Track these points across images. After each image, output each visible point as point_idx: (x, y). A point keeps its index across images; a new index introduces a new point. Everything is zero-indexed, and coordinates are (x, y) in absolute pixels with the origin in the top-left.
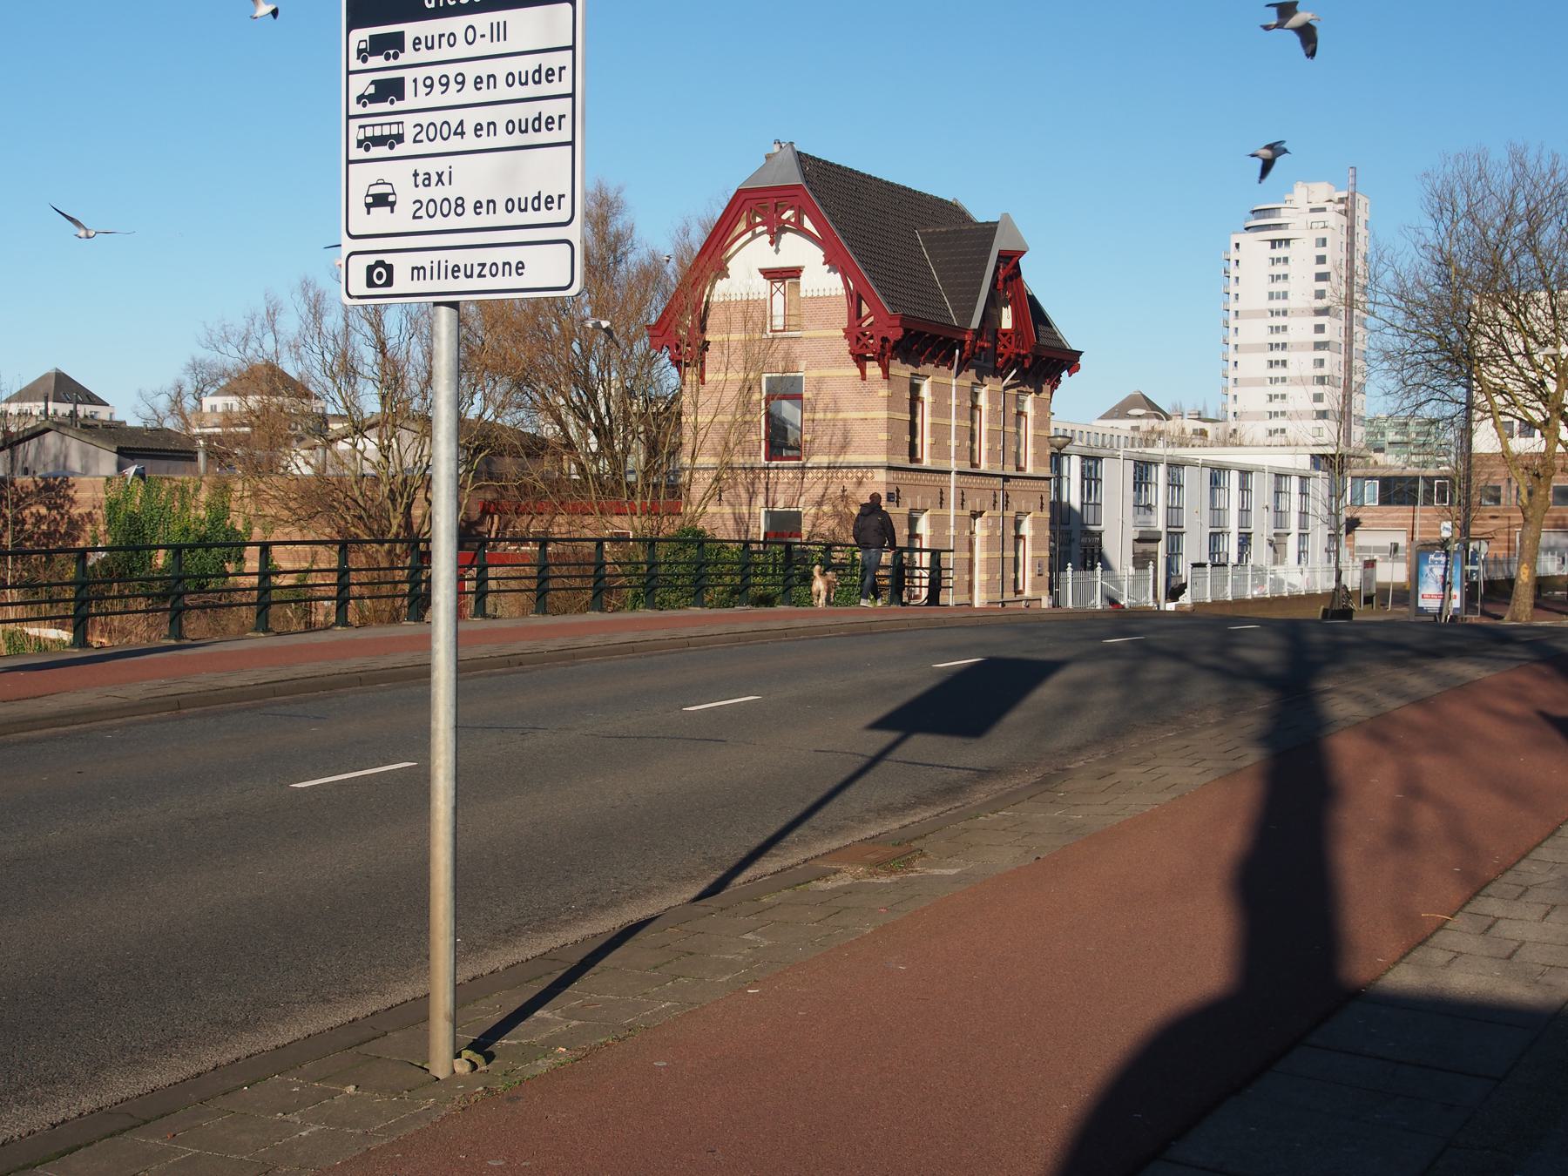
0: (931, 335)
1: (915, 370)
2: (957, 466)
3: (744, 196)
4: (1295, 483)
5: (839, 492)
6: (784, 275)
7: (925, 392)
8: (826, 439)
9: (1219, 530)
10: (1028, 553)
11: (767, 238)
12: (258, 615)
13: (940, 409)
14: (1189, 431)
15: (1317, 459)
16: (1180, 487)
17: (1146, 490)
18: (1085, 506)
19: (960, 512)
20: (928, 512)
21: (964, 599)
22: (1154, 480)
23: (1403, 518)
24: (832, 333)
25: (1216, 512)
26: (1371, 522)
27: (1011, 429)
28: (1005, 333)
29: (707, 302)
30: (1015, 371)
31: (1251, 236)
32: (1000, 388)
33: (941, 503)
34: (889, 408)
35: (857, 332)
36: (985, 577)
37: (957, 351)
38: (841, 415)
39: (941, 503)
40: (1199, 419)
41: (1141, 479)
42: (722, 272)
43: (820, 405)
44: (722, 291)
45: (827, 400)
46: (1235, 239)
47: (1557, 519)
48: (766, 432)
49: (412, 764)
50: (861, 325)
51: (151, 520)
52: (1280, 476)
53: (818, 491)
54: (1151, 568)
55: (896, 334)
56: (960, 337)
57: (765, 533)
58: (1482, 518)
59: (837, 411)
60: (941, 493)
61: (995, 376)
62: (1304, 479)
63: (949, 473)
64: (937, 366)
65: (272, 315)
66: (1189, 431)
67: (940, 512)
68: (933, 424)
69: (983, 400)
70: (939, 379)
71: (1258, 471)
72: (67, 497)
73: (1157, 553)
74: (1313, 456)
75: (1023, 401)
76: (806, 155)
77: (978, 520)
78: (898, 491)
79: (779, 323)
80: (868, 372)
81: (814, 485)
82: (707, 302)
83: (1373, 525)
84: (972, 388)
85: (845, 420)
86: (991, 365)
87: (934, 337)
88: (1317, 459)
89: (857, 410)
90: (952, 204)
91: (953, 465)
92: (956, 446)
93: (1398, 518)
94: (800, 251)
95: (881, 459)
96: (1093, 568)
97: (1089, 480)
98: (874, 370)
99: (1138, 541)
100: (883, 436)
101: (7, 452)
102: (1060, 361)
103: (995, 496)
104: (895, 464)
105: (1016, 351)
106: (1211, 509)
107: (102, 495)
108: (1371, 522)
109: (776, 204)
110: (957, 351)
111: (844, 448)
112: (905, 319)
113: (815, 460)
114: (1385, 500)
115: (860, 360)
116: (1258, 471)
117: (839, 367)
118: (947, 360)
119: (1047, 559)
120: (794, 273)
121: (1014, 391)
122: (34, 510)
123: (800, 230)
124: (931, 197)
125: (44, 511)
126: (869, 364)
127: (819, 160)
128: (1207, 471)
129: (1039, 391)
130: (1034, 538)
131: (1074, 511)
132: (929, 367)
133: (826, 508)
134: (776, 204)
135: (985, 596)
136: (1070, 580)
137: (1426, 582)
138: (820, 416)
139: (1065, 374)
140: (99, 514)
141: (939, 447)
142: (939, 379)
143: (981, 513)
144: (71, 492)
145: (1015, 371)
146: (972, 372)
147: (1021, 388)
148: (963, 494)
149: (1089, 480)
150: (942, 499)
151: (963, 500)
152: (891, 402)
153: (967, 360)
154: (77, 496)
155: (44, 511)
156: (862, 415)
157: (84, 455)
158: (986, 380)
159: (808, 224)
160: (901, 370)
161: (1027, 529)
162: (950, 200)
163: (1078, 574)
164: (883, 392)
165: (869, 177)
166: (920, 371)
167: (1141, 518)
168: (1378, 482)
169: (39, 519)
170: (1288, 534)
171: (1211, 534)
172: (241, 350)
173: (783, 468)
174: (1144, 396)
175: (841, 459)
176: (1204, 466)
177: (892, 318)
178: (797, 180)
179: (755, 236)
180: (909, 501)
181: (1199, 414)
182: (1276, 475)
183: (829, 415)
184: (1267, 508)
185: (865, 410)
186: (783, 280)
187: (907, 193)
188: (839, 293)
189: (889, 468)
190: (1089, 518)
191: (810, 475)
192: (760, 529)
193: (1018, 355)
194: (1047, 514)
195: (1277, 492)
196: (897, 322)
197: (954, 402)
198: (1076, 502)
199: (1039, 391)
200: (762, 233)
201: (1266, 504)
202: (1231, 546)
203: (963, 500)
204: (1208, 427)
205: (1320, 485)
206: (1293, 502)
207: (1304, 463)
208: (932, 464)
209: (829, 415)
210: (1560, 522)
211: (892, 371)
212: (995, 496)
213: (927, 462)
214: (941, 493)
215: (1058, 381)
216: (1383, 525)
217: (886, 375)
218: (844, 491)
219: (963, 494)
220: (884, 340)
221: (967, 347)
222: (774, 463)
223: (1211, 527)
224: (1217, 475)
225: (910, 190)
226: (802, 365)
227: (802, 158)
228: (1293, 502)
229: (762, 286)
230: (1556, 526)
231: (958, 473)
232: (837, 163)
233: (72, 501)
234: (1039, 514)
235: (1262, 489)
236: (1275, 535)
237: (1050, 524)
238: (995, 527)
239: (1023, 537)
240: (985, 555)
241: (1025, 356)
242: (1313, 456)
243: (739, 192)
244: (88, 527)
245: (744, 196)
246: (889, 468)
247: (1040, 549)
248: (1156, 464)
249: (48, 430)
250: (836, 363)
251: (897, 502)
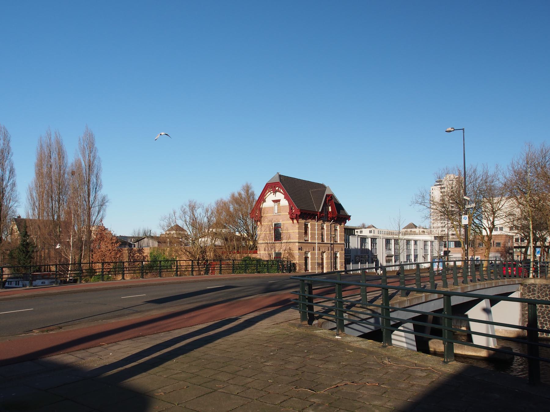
0: (308, 213)
1: (306, 221)
2: (317, 242)
3: (268, 185)
4: (429, 243)
5: (289, 248)
6: (277, 201)
7: (309, 226)
8: (285, 236)
9: (409, 254)
10: (338, 260)
11: (273, 193)
12: (142, 275)
13: (313, 229)
14: (421, 231)
15: (436, 238)
16: (417, 245)
17: (389, 245)
18: (373, 250)
19: (319, 252)
20: (310, 252)
21: (321, 271)
22: (391, 243)
23: (460, 250)
24: (286, 213)
25: (408, 250)
26: (452, 251)
27: (333, 233)
28: (330, 212)
29: (262, 208)
30: (333, 220)
31: (435, 187)
32: (329, 224)
33: (314, 250)
34: (298, 229)
35: (291, 213)
36: (326, 266)
37: (316, 217)
38: (289, 231)
39: (314, 250)
40: (423, 228)
41: (387, 243)
42: (264, 201)
43: (284, 230)
44: (264, 205)
45: (285, 228)
46: (432, 188)
47: (497, 250)
48: (274, 236)
49: (280, 307)
50: (292, 211)
51: (158, 256)
52: (425, 242)
53: (284, 248)
54: (391, 262)
55: (299, 213)
56: (317, 214)
57: (274, 257)
58: (479, 250)
59: (288, 230)
60: (314, 248)
61: (328, 222)
62: (432, 242)
63: (316, 243)
64: (312, 220)
65: (174, 213)
66: (421, 231)
67: (314, 252)
68: (311, 233)
69: (325, 227)
70: (312, 223)
71: (419, 240)
72: (143, 252)
73: (392, 259)
74: (435, 237)
75: (337, 227)
76: (282, 175)
77: (324, 253)
78: (302, 247)
79: (276, 212)
80: (294, 222)
81: (284, 246)
82: (262, 208)
83: (453, 252)
84: (322, 225)
85: (289, 232)
86: (327, 219)
87: (309, 214)
88: (436, 238)
89: (292, 230)
90: (321, 184)
91: (317, 242)
92: (317, 237)
93: (459, 250)
94: (280, 196)
95: (297, 241)
96: (366, 263)
97: (374, 243)
98: (295, 221)
99: (387, 257)
100: (297, 236)
101: (138, 242)
102: (345, 218)
103: (328, 248)
104: (300, 242)
105: (332, 216)
106: (386, 249)
107: (149, 251)
108: (452, 251)
109: (274, 186)
110: (316, 217)
111: (289, 238)
112: (300, 210)
113: (283, 241)
114: (456, 246)
115: (292, 219)
116: (419, 240)
117: (288, 221)
118: (314, 218)
119: (344, 262)
120: (279, 201)
121: (334, 225)
122: (137, 254)
123: (280, 192)
124: (316, 183)
125: (139, 255)
126: (294, 220)
127: (286, 176)
128: (405, 241)
129: (340, 225)
130: (340, 257)
131: (370, 250)
132: (310, 220)
133: (286, 252)
134: (274, 186)
135: (326, 270)
136: (351, 266)
137: (434, 266)
138: (284, 232)
139: (347, 220)
140: (149, 255)
141: (313, 237)
142: (312, 223)
143: (325, 252)
144: (143, 251)
145: (333, 220)
146: (321, 221)
147: (335, 224)
148: (319, 248)
149: (374, 243)
150: (314, 249)
151: (319, 249)
152: (299, 228)
153: (319, 218)
154: (145, 252)
155: (139, 255)
156: (293, 231)
157: (153, 243)
158: (325, 222)
159: (281, 191)
160: (302, 221)
161: (338, 255)
162: (322, 183)
163: (353, 265)
164: (297, 226)
165: (299, 179)
166: (307, 221)
167: (387, 252)
168: (454, 242)
169: (138, 256)
170: (428, 255)
171: (407, 255)
172: (168, 220)
173: (277, 243)
174: (413, 224)
175: (289, 241)
176: (404, 240)
177: (298, 210)
178: (278, 181)
179: (271, 193)
180: (305, 250)
181: (423, 227)
182: (424, 241)
183: (286, 231)
184: (422, 249)
185: (294, 230)
186: (277, 202)
187: (309, 182)
188: (287, 205)
189: (299, 243)
190: (374, 251)
191: (283, 244)
192: (273, 256)
193: (333, 217)
194: (343, 252)
195: (425, 245)
196: (299, 211)
197: (316, 228)
198: (370, 248)
199: (340, 225)
200: (272, 193)
201: (422, 248)
202: (412, 258)
203: (319, 249)
204: (425, 230)
205: (436, 243)
206: (429, 248)
207: (433, 238)
208: (311, 241)
209: (286, 231)
210: (498, 251)
211: (299, 221)
212: (328, 248)
213: (325, 242)
214: (314, 248)
215: (346, 222)
216: (456, 252)
217: (298, 222)
218: (290, 248)
219: (319, 248)
220: (297, 215)
221: (318, 216)
222: (276, 242)
223: (361, 253)
224: (408, 242)
225: (310, 182)
226: (281, 221)
227: (280, 176)
228: (429, 248)
229: (273, 203)
230: (497, 252)
231: (318, 243)
232: (290, 177)
233: (144, 253)
234: (341, 252)
235: (420, 245)
236: (424, 255)
237: (345, 254)
238: (328, 255)
239: (337, 257)
240: (326, 261)
241: (335, 217)
242: (435, 237)
243: (267, 184)
244: (147, 258)
245: (268, 185)
246: (299, 243)
247: (342, 260)
248: (391, 239)
249: (145, 238)
250: (288, 220)
251: (302, 250)
